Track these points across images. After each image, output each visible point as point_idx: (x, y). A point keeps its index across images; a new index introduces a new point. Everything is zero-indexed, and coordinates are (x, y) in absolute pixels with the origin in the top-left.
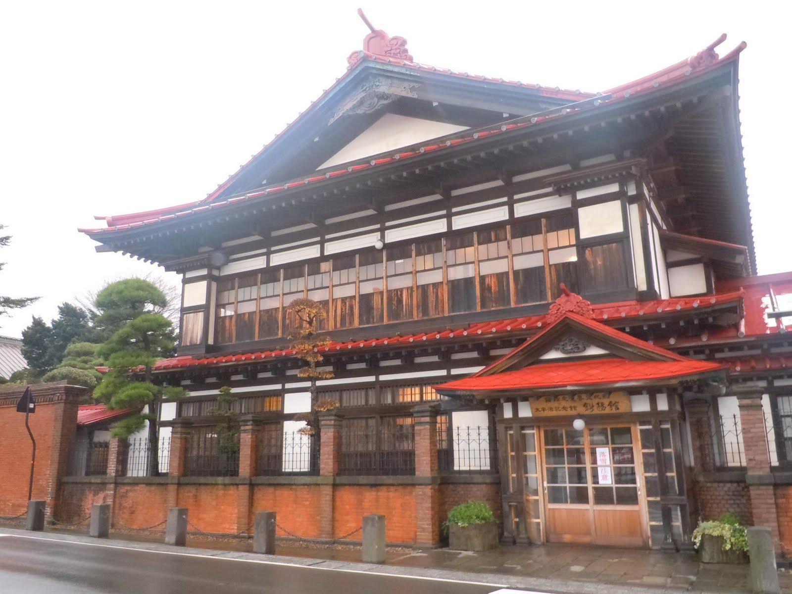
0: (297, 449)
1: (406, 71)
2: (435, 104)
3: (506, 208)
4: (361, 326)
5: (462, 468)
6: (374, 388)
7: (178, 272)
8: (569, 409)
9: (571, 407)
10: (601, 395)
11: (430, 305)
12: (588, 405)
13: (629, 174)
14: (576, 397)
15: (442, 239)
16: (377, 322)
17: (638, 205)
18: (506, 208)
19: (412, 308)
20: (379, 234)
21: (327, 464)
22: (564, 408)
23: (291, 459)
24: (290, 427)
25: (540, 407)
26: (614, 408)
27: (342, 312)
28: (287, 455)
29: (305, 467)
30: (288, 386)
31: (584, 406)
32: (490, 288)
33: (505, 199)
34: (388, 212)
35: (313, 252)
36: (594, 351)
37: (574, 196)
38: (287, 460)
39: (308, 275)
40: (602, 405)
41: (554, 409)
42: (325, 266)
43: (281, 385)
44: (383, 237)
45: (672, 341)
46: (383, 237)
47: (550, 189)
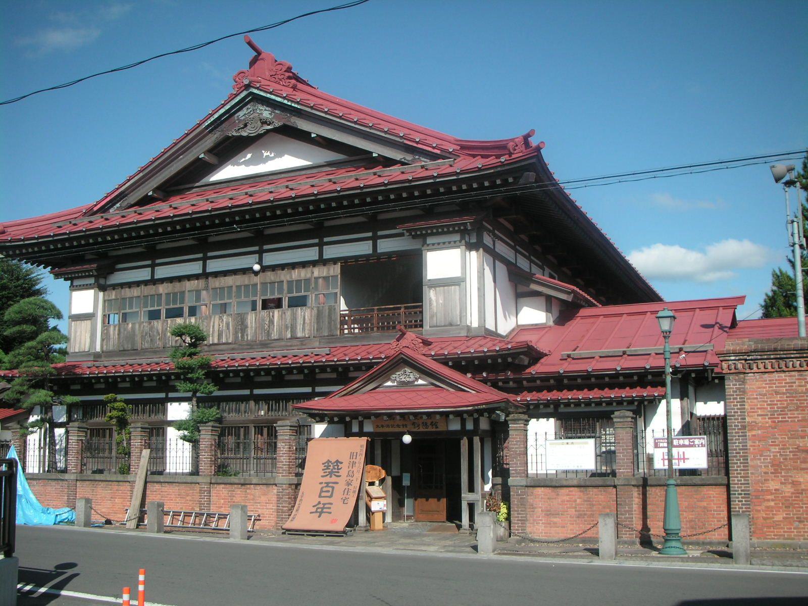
0: (180, 454)
2: (313, 135)
5: (171, 471)
7: (66, 279)
8: (401, 427)
9: (403, 425)
21: (206, 466)
23: (181, 462)
24: (172, 433)
27: (219, 328)
28: (30, 457)
29: (187, 468)
34: (210, 242)
38: (30, 460)
43: (311, 388)
45: (484, 374)
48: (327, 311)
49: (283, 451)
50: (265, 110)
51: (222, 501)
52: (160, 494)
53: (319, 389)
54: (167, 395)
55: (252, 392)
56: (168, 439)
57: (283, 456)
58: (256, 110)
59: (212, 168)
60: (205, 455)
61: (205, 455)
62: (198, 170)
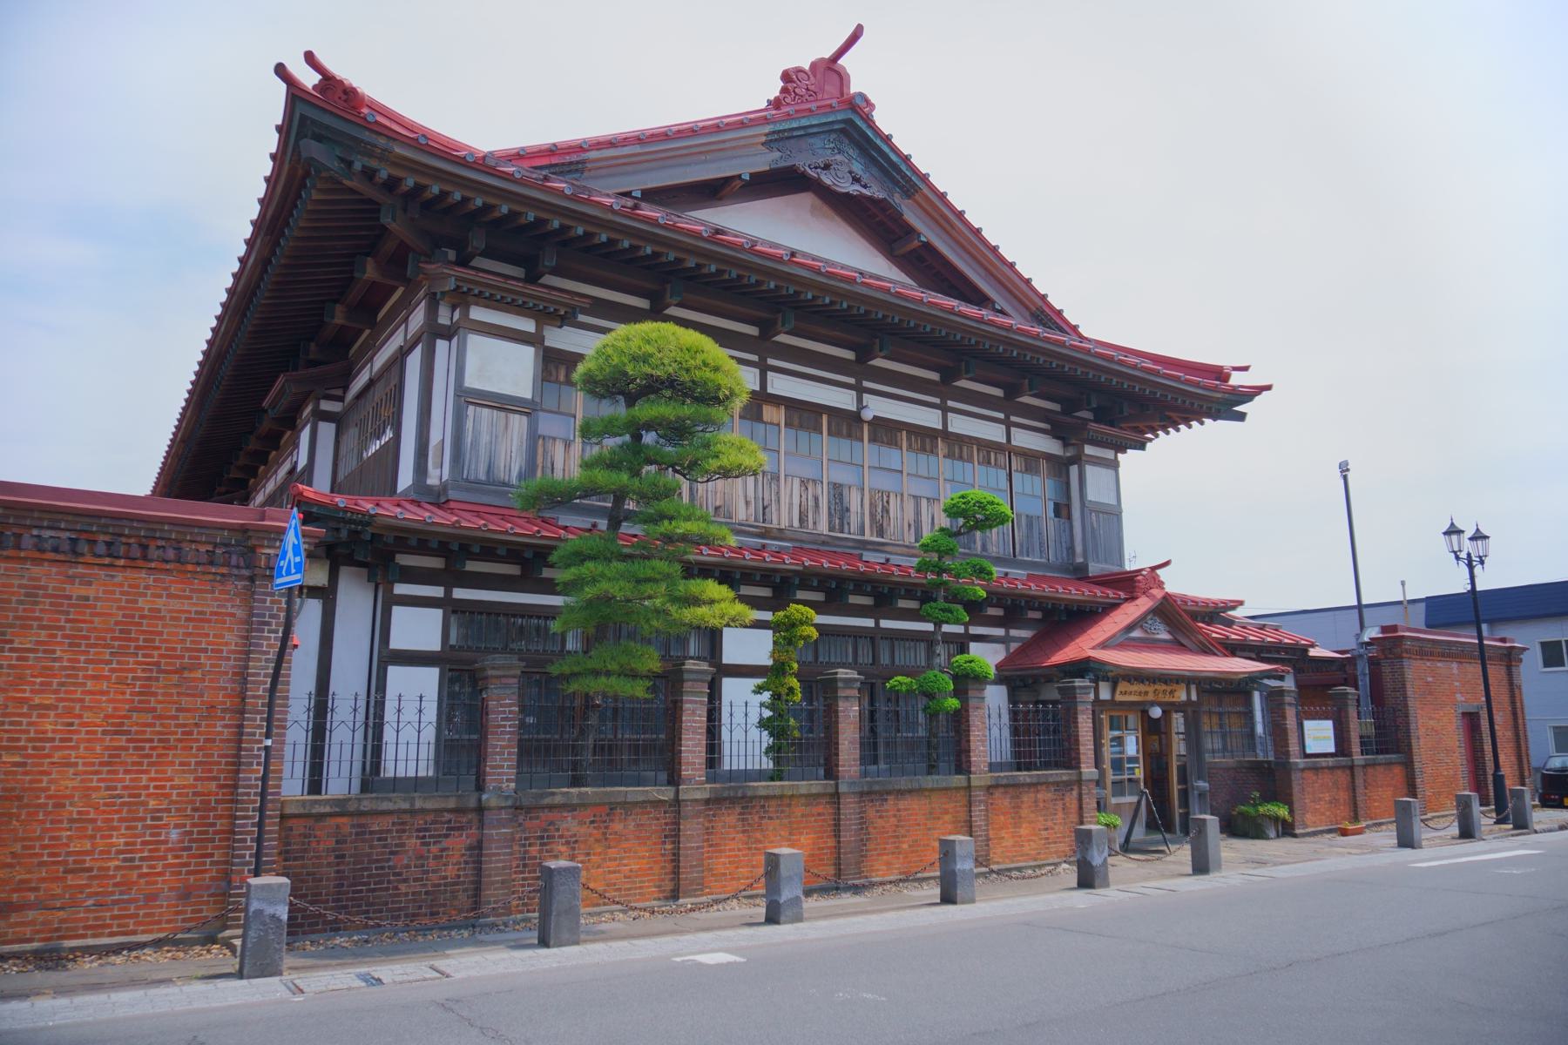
55: (448, 592)
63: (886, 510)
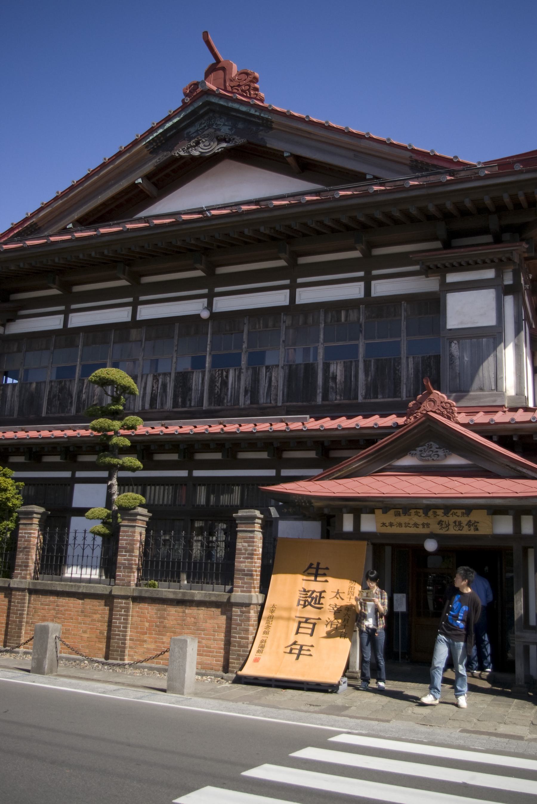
0: (88, 551)
1: (256, 111)
3: (362, 284)
4: (175, 410)
6: (186, 485)
8: (421, 526)
10: (459, 512)
11: (261, 392)
12: (444, 523)
13: (509, 259)
14: (430, 513)
15: (282, 314)
16: (194, 407)
17: (514, 298)
18: (362, 284)
19: (239, 392)
20: (205, 300)
21: (216, 592)
22: (416, 525)
25: (387, 522)
26: (472, 528)
27: (152, 390)
30: (79, 474)
31: (438, 524)
32: (334, 378)
33: (361, 274)
35: (122, 315)
36: (455, 460)
37: (444, 278)
39: (114, 343)
40: (460, 523)
41: (403, 525)
42: (134, 333)
44: (210, 306)
46: (210, 306)
47: (417, 268)
48: (302, 371)
49: (245, 554)
50: (224, 125)
51: (147, 624)
52: (54, 609)
53: (285, 473)
54: (73, 474)
55: (190, 473)
56: (72, 530)
57: (244, 562)
58: (213, 125)
59: (148, 200)
60: (125, 556)
61: (125, 556)
62: (133, 200)
63: (225, 383)
